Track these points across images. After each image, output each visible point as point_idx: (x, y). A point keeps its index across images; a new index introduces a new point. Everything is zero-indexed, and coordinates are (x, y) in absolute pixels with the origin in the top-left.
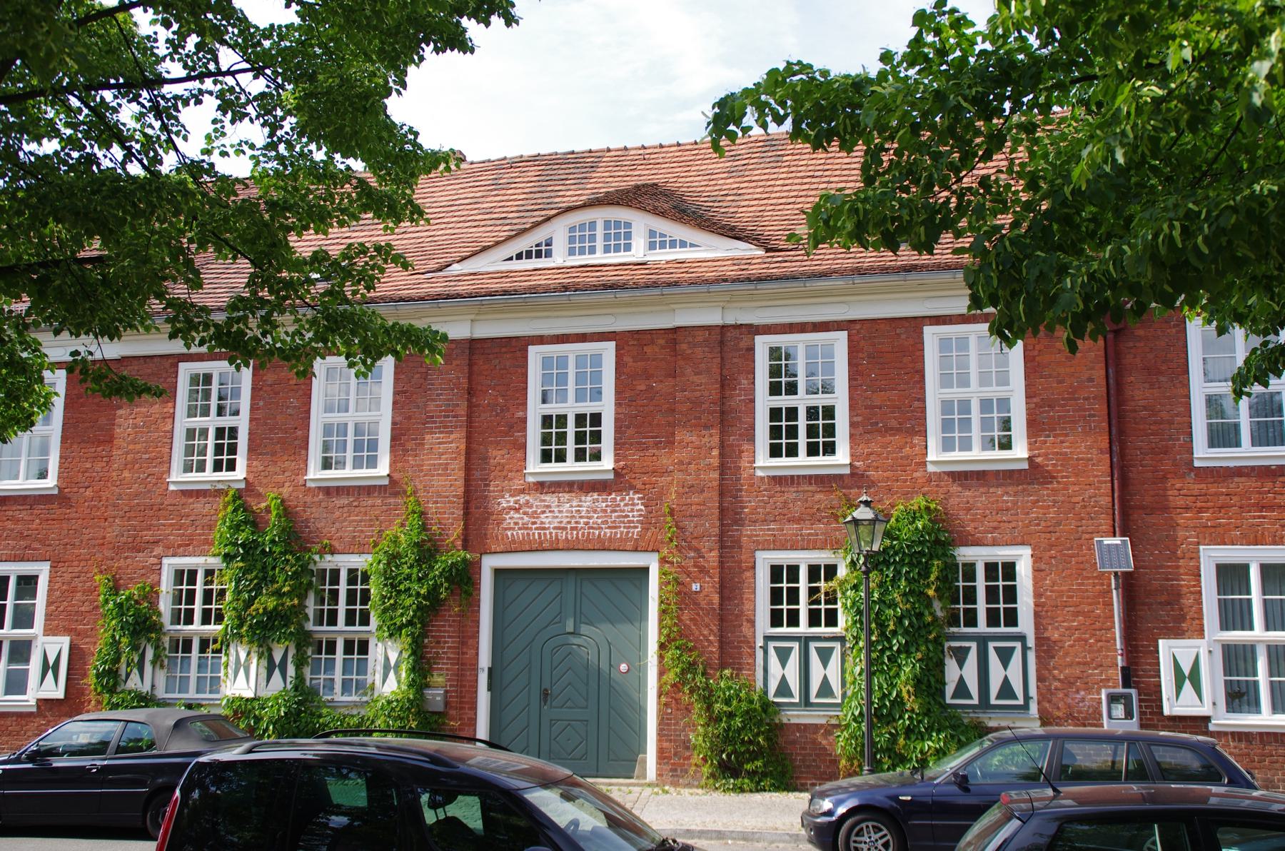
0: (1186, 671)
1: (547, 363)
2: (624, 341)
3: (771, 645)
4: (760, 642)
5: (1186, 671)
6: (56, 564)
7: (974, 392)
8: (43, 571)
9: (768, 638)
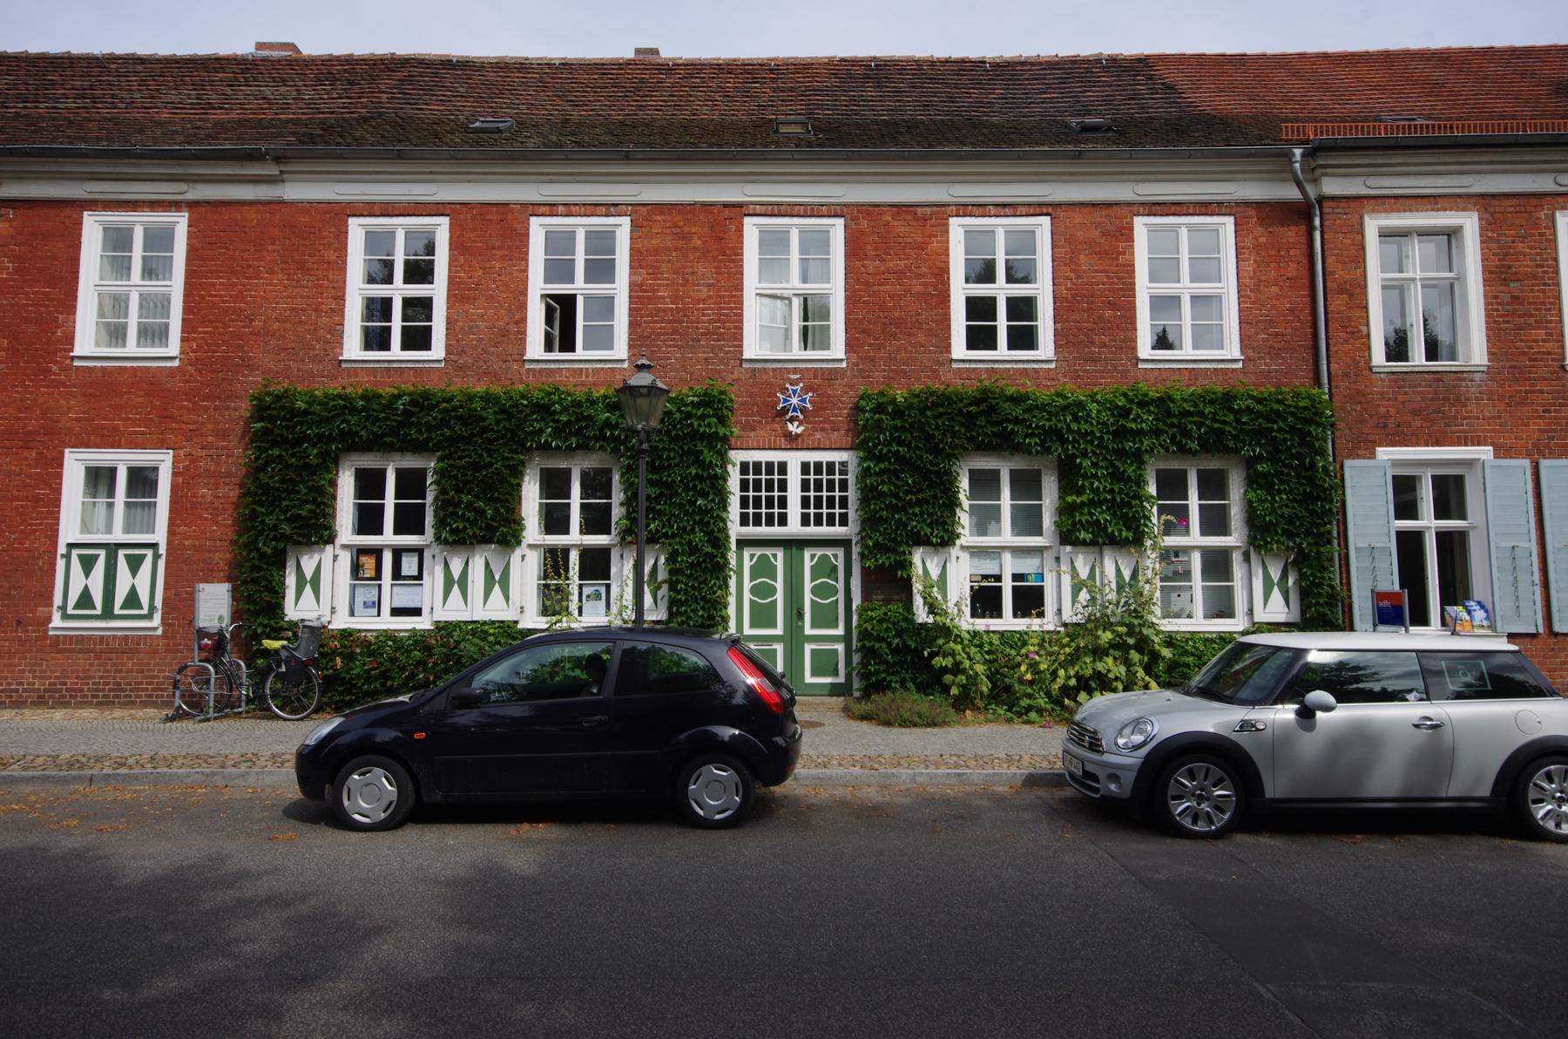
0: (308, 588)
3: (75, 552)
4: (62, 549)
5: (308, 588)
8: (164, 462)
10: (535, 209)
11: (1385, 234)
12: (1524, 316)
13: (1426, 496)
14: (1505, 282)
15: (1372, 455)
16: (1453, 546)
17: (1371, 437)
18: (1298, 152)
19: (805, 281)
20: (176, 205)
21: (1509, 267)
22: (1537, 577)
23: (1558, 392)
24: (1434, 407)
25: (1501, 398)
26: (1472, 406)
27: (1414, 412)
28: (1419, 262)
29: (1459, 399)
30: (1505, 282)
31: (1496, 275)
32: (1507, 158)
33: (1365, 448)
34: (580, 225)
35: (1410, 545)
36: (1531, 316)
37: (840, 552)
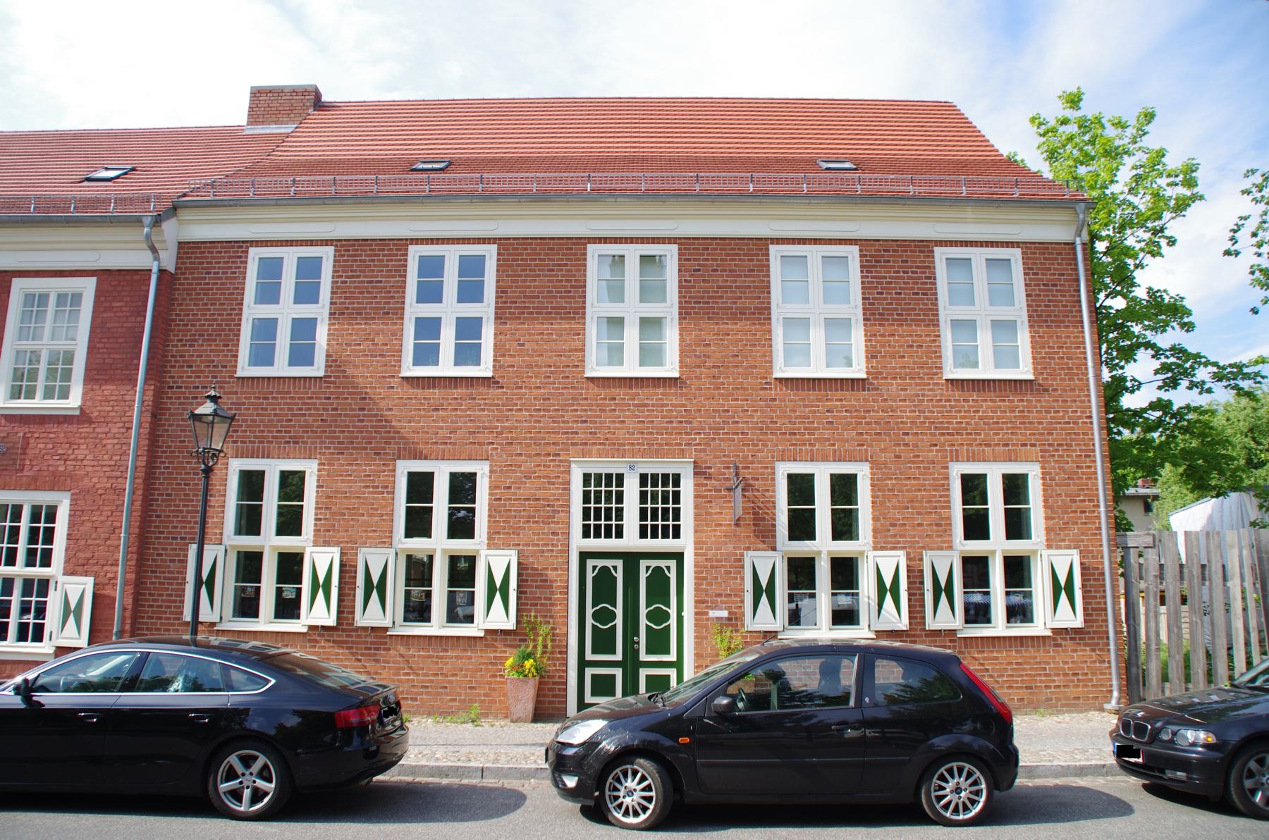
1: (29, 298)
2: (685, 244)
6: (875, 466)
7: (46, 344)
9: (584, 556)
20: (326, 242)
37: (590, 563)
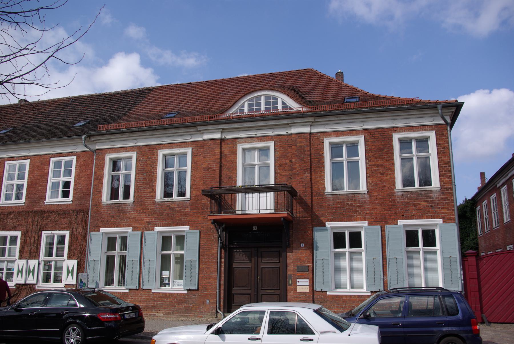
10: (396, 130)
11: (244, 150)
12: (146, 184)
13: (118, 242)
14: (142, 174)
15: (99, 231)
16: (123, 259)
17: (99, 225)
18: (83, 137)
19: (126, 170)
21: (144, 169)
22: (138, 271)
23: (153, 209)
24: (117, 216)
25: (137, 211)
26: (128, 215)
27: (113, 216)
28: (255, 158)
29: (124, 212)
30: (142, 174)
31: (139, 171)
32: (415, 113)
33: (96, 228)
34: (63, 159)
35: (110, 260)
36: (148, 184)
